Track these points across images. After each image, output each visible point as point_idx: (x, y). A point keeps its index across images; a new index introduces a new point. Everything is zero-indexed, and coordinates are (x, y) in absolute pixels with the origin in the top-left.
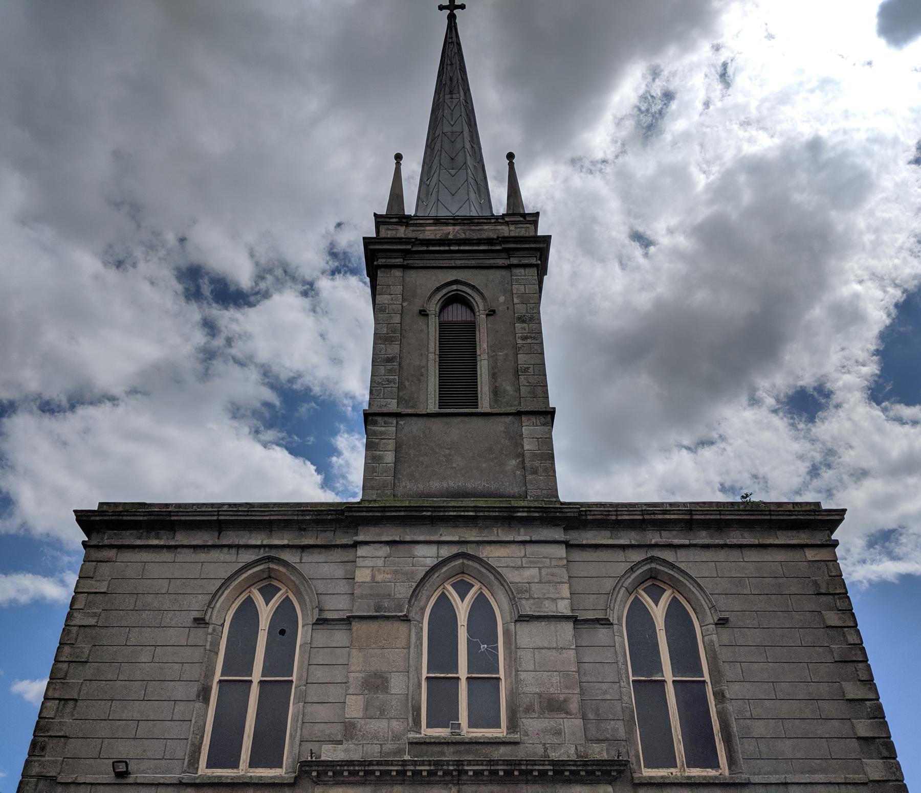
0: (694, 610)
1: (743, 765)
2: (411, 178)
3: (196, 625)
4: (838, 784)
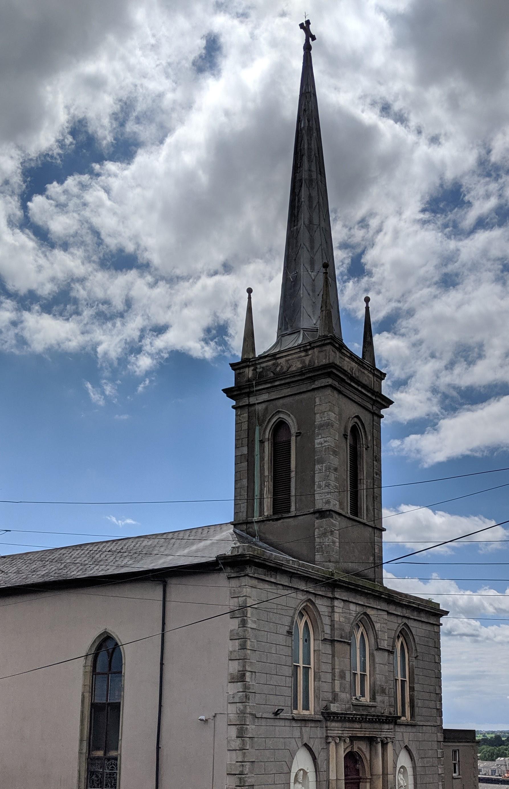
0: (313, 627)
1: (417, 718)
2: (266, 311)
3: (288, 635)
4: (431, 726)
